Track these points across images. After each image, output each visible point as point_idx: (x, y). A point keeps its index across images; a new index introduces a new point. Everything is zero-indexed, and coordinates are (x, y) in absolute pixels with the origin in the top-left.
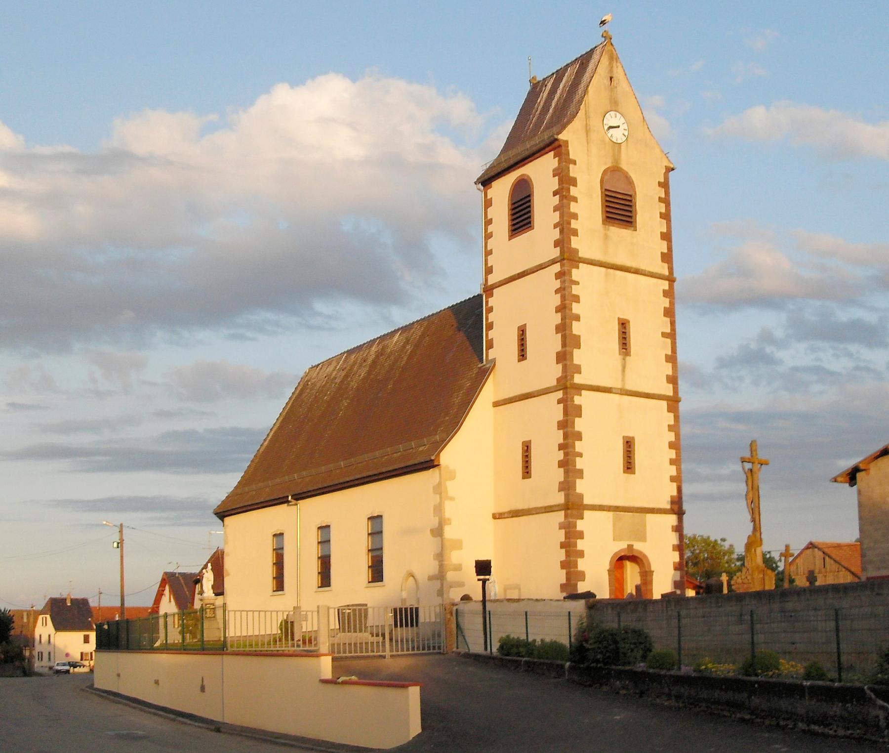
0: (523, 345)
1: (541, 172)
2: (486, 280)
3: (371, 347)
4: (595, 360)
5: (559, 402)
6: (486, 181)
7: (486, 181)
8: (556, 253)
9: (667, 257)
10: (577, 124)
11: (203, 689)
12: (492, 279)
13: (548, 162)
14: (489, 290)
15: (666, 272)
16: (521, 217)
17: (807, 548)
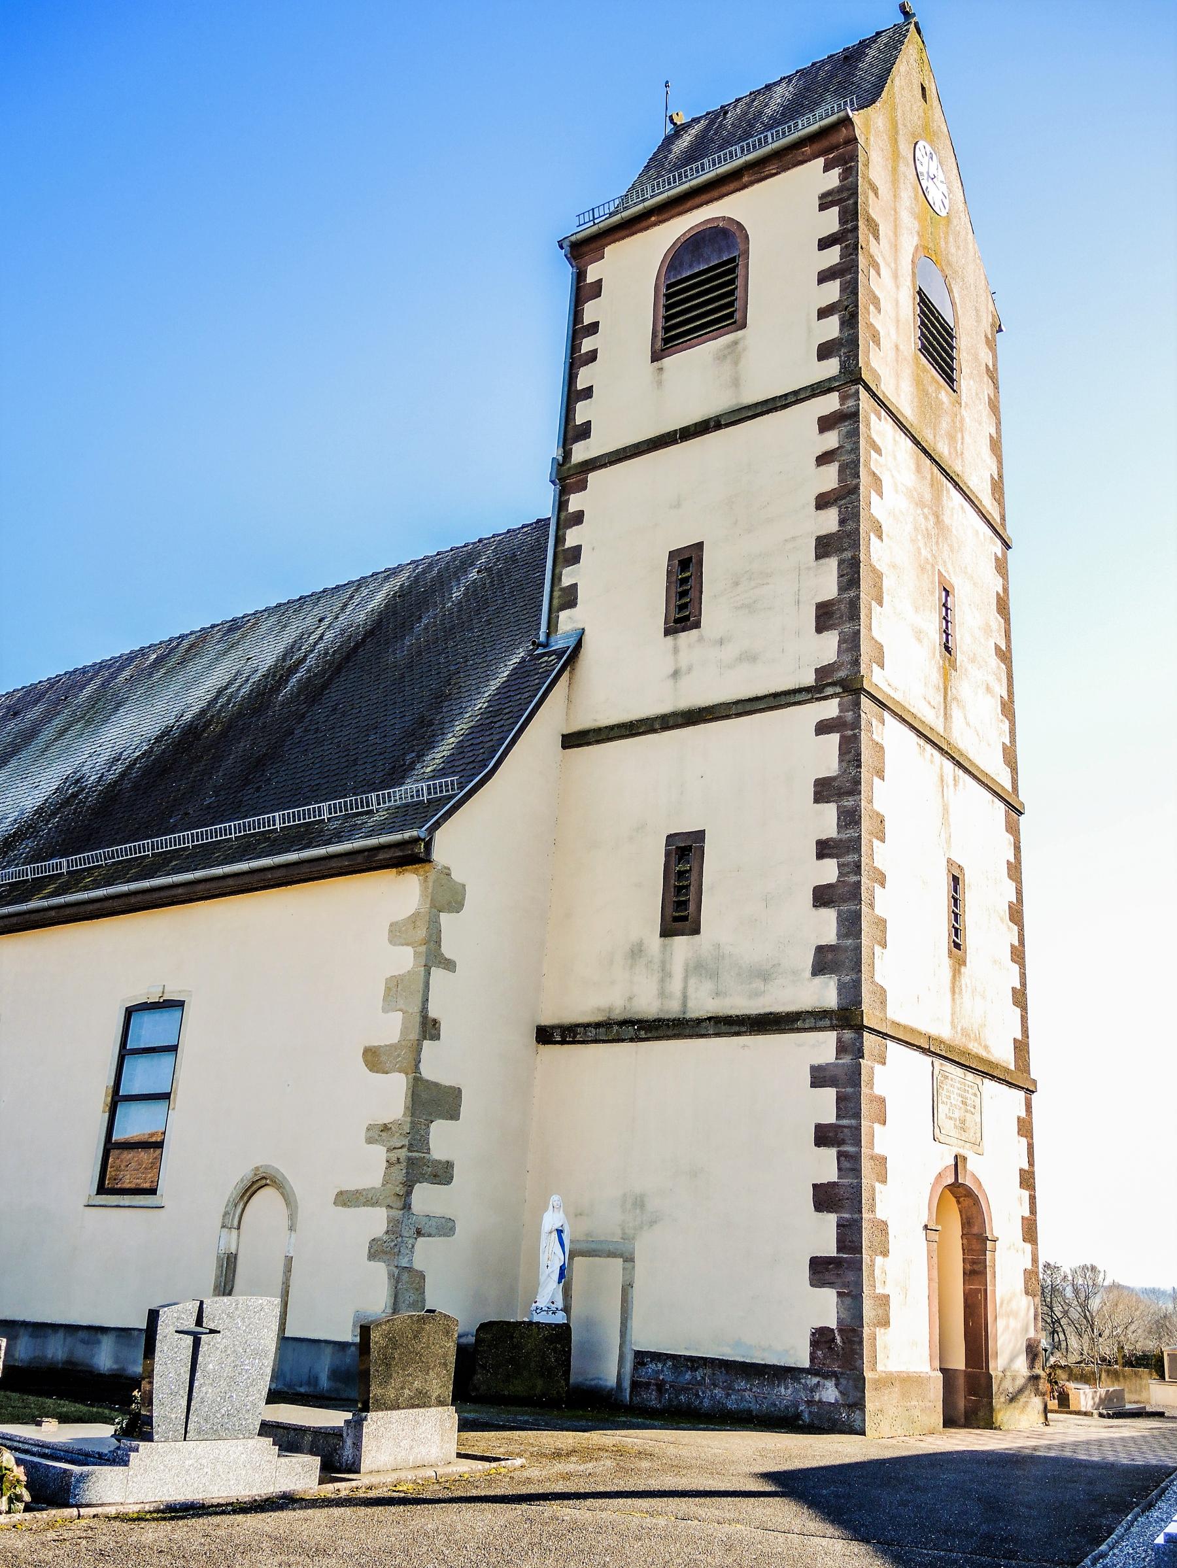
2: (567, 454)
3: (121, 669)
7: (582, 250)
8: (832, 367)
13: (815, 176)
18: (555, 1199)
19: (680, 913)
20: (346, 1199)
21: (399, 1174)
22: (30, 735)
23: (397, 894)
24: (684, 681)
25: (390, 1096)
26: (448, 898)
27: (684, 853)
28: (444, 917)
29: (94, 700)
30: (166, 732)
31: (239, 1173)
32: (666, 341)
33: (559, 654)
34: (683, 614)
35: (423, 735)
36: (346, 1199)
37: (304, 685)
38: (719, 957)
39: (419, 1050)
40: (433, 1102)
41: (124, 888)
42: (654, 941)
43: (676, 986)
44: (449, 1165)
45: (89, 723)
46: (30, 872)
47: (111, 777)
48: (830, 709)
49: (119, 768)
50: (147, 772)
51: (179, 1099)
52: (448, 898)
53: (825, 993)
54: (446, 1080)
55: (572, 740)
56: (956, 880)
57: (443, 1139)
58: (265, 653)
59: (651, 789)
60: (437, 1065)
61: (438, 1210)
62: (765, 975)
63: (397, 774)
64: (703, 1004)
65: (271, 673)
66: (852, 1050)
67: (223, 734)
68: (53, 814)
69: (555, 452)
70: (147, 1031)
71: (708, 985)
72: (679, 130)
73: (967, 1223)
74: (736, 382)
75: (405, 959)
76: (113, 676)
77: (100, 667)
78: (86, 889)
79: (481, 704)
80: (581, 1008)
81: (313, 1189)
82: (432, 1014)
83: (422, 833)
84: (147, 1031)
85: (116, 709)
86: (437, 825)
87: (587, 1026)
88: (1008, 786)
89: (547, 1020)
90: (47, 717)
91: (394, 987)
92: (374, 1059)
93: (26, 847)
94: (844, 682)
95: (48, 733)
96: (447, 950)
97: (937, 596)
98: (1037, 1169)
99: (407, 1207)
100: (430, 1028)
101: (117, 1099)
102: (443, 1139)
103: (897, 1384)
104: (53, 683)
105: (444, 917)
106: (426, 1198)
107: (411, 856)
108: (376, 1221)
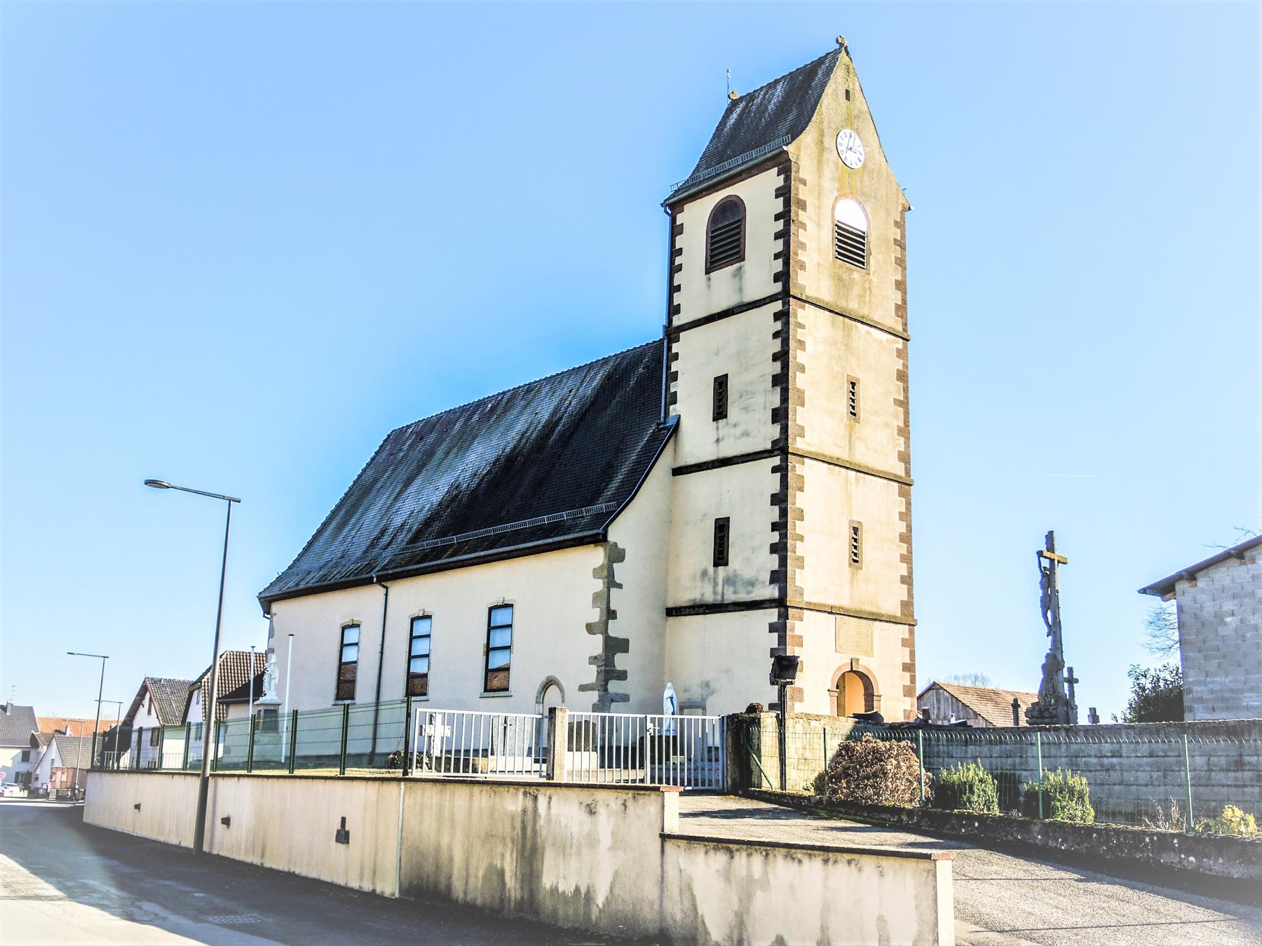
0: (720, 400)
1: (757, 193)
2: (670, 321)
3: (474, 413)
4: (815, 424)
5: (775, 470)
6: (674, 206)
7: (674, 206)
8: (778, 287)
9: (901, 310)
10: (808, 137)
11: (343, 836)
12: (678, 321)
13: (771, 179)
14: (672, 334)
15: (899, 328)
16: (726, 244)
17: (929, 689)
18: (669, 684)
19: (721, 558)
20: (583, 688)
21: (602, 677)
22: (430, 454)
23: (595, 556)
24: (721, 444)
25: (596, 644)
26: (617, 555)
27: (722, 527)
28: (615, 565)
29: (462, 432)
30: (497, 460)
31: (541, 679)
32: (712, 263)
33: (668, 429)
34: (720, 412)
35: (609, 472)
36: (583, 688)
37: (562, 434)
38: (736, 576)
39: (607, 624)
40: (615, 646)
41: (482, 553)
42: (711, 569)
43: (720, 589)
44: (625, 672)
45: (460, 449)
46: (439, 542)
47: (473, 486)
48: (776, 461)
49: (476, 480)
50: (490, 483)
51: (515, 648)
52: (617, 555)
53: (772, 592)
54: (621, 636)
55: (678, 471)
56: (856, 530)
57: (621, 661)
58: (544, 410)
59: (707, 495)
60: (615, 630)
61: (621, 691)
62: (752, 584)
63: (592, 502)
64: (730, 597)
65: (548, 422)
66: (784, 616)
67: (524, 463)
68: (447, 507)
69: (664, 322)
70: (498, 618)
71: (731, 589)
72: (734, 103)
73: (866, 689)
74: (741, 290)
75: (599, 585)
76: (470, 417)
77: (463, 409)
78: (465, 553)
79: (634, 457)
80: (685, 597)
81: (571, 687)
82: (612, 607)
83: (600, 531)
84: (498, 618)
85: (472, 442)
86: (608, 526)
87: (685, 608)
88: (902, 474)
89: (670, 605)
90: (439, 441)
91: (596, 597)
92: (590, 628)
93: (436, 526)
94: (780, 448)
95: (440, 453)
96: (617, 579)
97: (847, 387)
98: (917, 662)
99: (606, 690)
100: (611, 614)
101: (489, 650)
102: (621, 661)
103: (802, 751)
104: (439, 417)
105: (615, 565)
106: (614, 686)
107: (600, 539)
108: (594, 696)
